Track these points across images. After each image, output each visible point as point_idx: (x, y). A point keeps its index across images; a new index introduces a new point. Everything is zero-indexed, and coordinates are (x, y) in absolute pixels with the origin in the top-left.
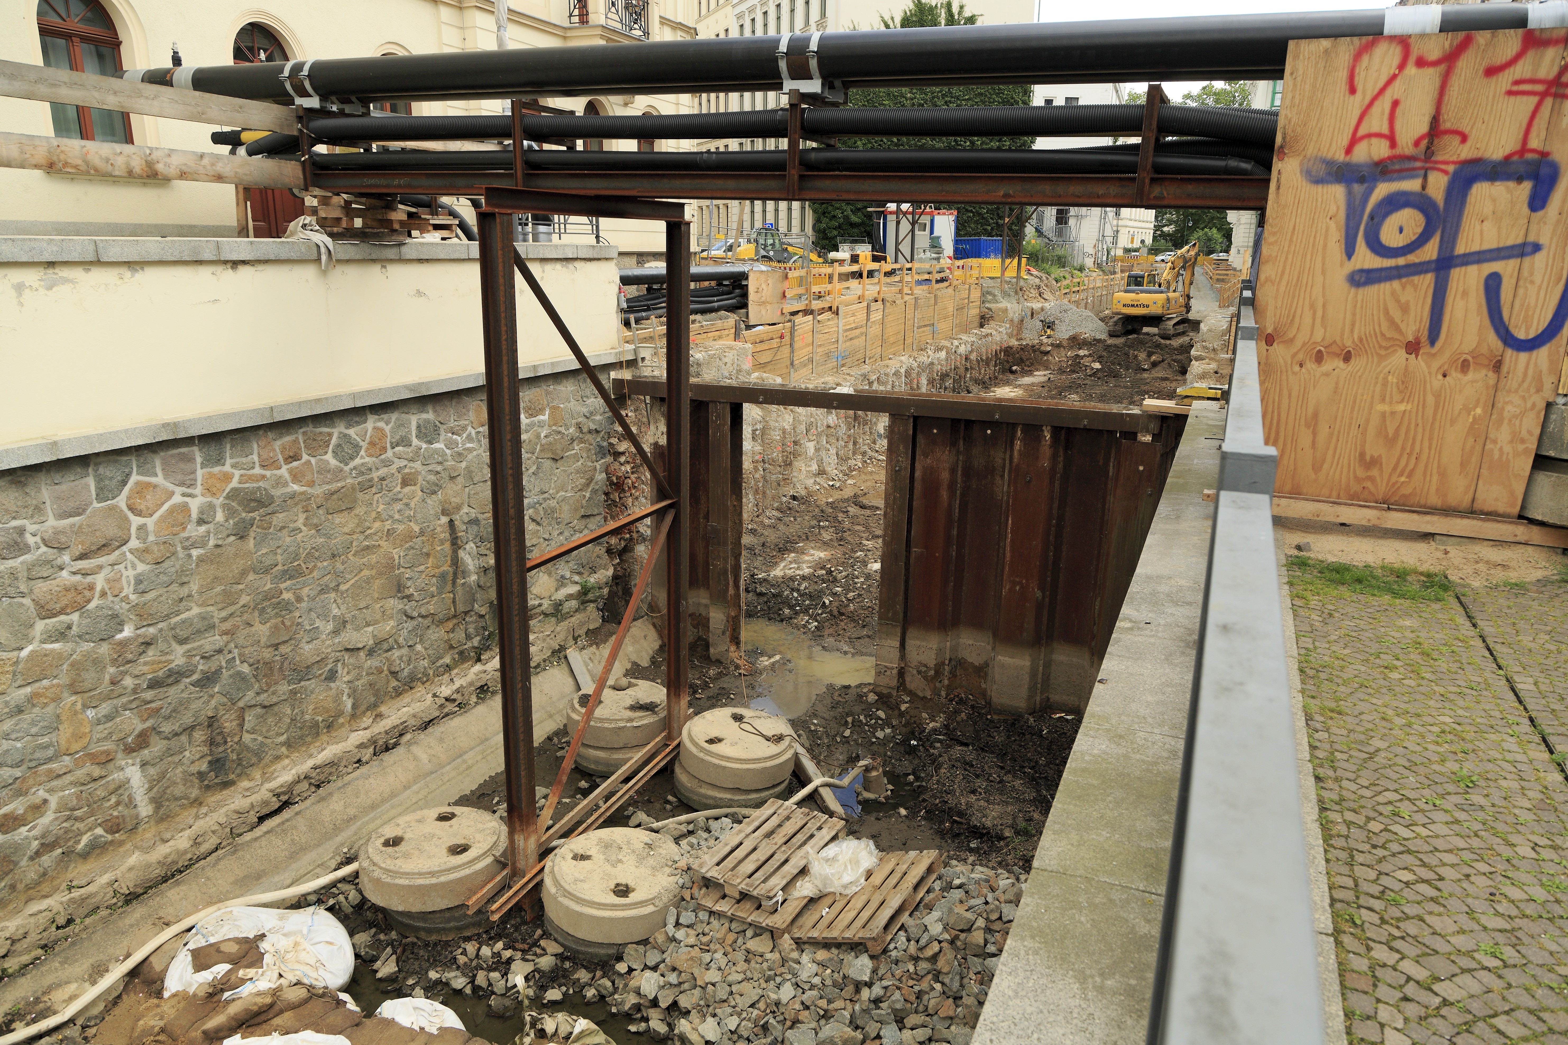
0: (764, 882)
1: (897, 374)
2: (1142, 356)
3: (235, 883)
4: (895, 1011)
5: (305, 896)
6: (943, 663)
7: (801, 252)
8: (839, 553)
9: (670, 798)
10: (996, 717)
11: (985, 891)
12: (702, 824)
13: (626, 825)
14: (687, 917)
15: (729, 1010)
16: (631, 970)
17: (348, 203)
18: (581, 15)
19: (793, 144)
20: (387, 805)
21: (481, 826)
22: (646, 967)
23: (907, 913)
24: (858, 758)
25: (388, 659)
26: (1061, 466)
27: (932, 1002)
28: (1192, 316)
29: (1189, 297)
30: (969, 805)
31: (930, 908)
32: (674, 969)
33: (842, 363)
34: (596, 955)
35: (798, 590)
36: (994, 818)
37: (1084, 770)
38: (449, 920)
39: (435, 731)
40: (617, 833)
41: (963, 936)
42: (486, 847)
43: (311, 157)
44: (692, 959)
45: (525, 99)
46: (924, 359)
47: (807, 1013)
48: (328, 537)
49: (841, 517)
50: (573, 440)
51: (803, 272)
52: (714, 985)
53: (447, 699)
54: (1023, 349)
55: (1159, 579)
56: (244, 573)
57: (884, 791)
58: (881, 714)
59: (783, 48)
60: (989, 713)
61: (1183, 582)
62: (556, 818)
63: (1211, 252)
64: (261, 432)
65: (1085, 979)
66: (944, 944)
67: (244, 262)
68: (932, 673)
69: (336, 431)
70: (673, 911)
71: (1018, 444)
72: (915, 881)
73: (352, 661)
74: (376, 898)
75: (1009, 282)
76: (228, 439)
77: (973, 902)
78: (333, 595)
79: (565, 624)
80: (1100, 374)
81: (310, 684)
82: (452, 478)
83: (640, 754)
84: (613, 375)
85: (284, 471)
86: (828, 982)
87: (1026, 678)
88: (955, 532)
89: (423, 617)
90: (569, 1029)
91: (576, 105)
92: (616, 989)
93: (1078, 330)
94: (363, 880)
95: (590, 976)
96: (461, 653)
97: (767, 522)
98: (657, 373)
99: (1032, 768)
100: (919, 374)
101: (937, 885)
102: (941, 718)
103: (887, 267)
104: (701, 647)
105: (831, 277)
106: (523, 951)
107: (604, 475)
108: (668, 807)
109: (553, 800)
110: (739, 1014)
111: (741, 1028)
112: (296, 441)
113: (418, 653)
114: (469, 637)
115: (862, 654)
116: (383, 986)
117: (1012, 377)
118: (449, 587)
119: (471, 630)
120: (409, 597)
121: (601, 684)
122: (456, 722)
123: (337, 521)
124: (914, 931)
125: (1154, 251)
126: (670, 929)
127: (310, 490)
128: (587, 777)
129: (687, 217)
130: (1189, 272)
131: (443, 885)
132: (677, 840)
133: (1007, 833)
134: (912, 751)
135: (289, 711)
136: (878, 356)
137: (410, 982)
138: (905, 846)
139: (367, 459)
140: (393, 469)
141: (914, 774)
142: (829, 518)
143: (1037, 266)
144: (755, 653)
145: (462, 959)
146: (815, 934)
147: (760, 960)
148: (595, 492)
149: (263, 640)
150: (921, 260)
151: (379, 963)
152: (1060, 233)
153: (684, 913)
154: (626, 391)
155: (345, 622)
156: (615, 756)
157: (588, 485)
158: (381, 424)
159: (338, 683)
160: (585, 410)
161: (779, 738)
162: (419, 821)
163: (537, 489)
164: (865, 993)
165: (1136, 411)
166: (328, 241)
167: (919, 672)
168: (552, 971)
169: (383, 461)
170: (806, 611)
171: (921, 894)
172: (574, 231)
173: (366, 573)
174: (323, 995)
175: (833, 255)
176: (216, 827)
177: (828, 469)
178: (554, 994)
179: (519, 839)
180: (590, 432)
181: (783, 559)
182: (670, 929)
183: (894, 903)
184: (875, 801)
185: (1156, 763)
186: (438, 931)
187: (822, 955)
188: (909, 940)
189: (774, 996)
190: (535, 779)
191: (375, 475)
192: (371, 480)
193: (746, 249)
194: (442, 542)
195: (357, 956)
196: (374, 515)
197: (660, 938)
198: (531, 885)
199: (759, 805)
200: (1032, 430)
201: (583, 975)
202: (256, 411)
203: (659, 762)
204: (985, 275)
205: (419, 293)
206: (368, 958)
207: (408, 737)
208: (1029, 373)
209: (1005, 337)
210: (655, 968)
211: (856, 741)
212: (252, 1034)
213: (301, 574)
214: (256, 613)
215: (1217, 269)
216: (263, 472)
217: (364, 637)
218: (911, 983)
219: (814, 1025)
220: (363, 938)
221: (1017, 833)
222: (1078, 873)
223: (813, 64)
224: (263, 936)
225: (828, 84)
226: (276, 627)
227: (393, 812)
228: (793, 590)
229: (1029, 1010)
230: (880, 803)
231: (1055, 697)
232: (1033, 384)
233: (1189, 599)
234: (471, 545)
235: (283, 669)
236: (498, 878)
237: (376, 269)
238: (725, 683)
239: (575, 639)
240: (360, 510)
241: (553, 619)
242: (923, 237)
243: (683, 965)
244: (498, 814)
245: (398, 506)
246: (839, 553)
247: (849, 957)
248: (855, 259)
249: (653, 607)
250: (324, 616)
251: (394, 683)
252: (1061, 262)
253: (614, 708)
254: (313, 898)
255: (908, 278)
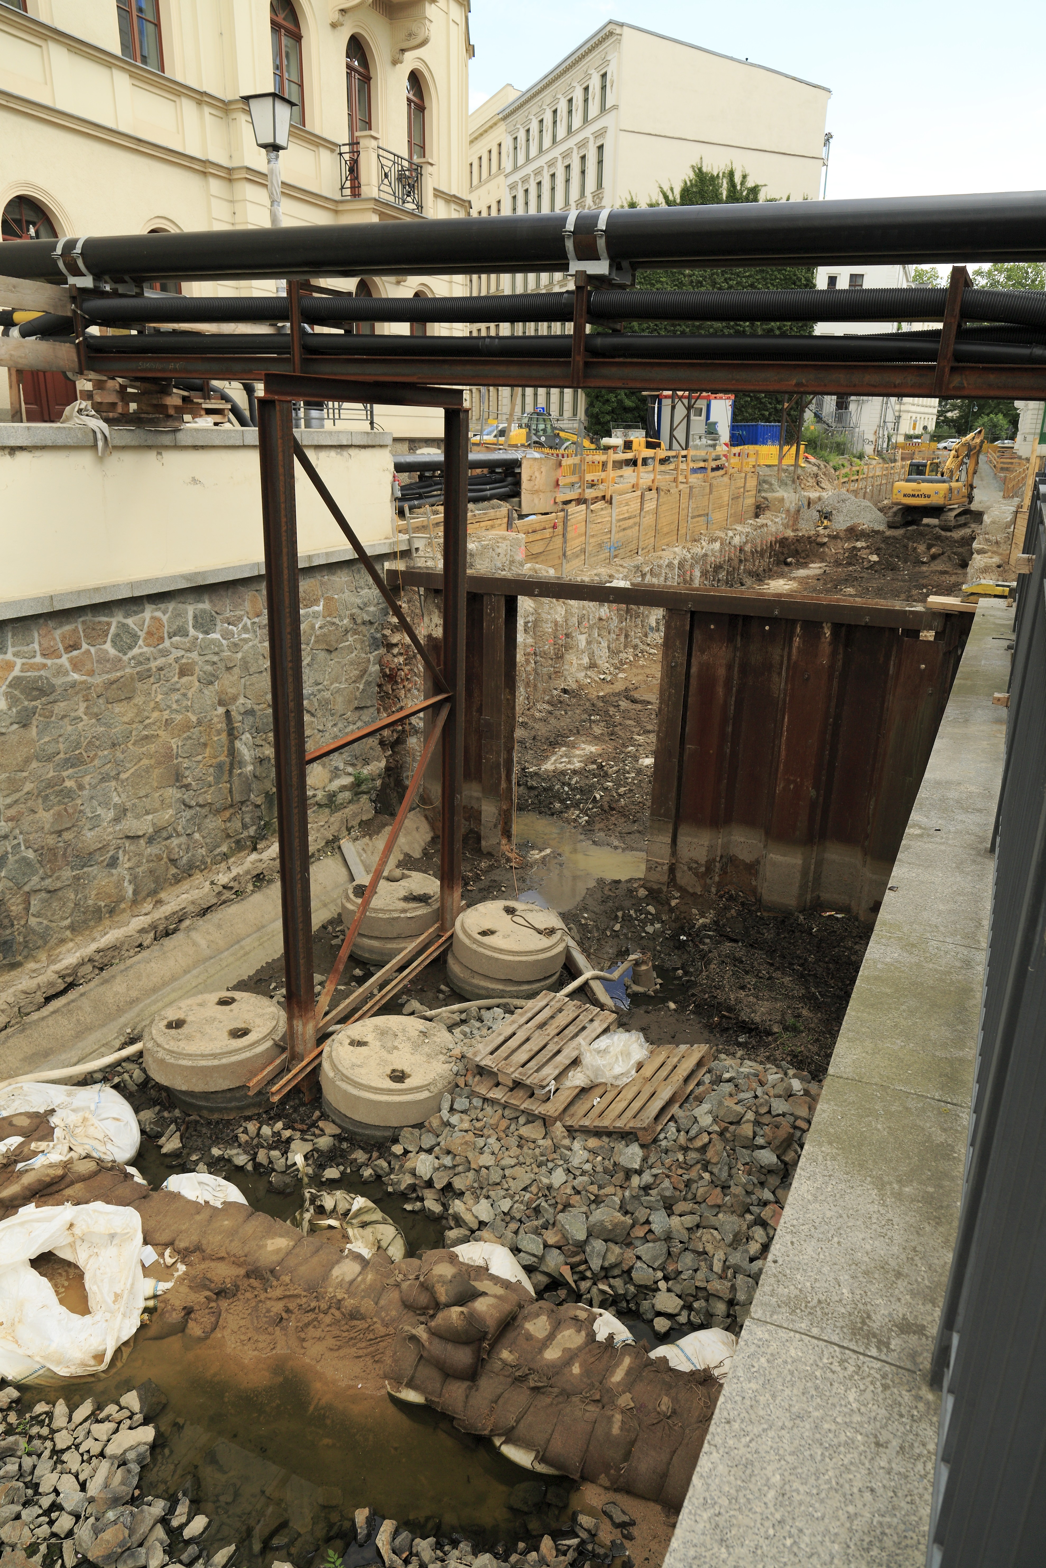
0: (537, 1071)
1: (670, 565)
2: (921, 548)
3: (24, 1060)
4: (664, 1198)
5: (91, 1073)
6: (714, 860)
7: (575, 438)
8: (610, 747)
9: (443, 987)
10: (765, 914)
11: (754, 1085)
12: (474, 1014)
13: (399, 1013)
14: (461, 1103)
15: (503, 1193)
16: (406, 1152)
17: (123, 388)
18: (352, 188)
19: (579, 329)
20: (168, 988)
21: (260, 1011)
22: (421, 1149)
23: (677, 1105)
24: (627, 952)
25: (167, 847)
26: (840, 663)
27: (701, 1191)
28: (974, 507)
29: (972, 487)
30: (738, 1001)
31: (700, 1100)
32: (448, 1152)
33: (614, 553)
34: (373, 1137)
35: (569, 785)
36: (763, 1014)
37: (876, 978)
38: (231, 1100)
39: (214, 917)
40: (392, 1021)
41: (732, 1128)
42: (265, 1030)
43: (85, 339)
44: (466, 1143)
45: (297, 278)
46: (698, 550)
47: (578, 1197)
48: (109, 726)
49: (612, 711)
50: (347, 631)
51: (576, 460)
52: (487, 1168)
53: (224, 887)
54: (799, 540)
55: (948, 784)
56: (27, 761)
57: (653, 984)
58: (651, 909)
59: (570, 226)
60: (759, 910)
61: (972, 788)
62: (333, 1005)
63: (996, 439)
64: (41, 621)
65: (883, 1185)
66: (714, 1136)
67: (21, 448)
68: (703, 869)
69: (115, 621)
70: (448, 1097)
71: (797, 640)
72: (685, 1074)
73: (132, 848)
74: (160, 1077)
75: (786, 471)
76: (9, 628)
77: (742, 1096)
78: (113, 784)
79: (338, 815)
80: (877, 567)
81: (93, 870)
82: (228, 669)
83: (414, 944)
84: (387, 565)
85: (64, 660)
86: (599, 1169)
87: (798, 876)
88: (730, 729)
89: (201, 806)
90: (347, 1206)
91: (347, 284)
92: (392, 1170)
93: (856, 521)
94: (148, 1060)
95: (367, 1156)
96: (238, 842)
97: (538, 715)
98: (430, 564)
99: (801, 965)
100: (692, 566)
101: (707, 1079)
102: (711, 914)
103: (662, 453)
104: (474, 839)
105: (604, 465)
106: (303, 1132)
107: (377, 667)
108: (441, 996)
109: (330, 987)
110: (512, 1197)
111: (514, 1210)
112: (75, 630)
113: (196, 841)
114: (245, 826)
115: (633, 849)
116: (167, 1161)
117: (786, 569)
118: (226, 777)
119: (247, 820)
120: (187, 787)
121: (377, 877)
122: (233, 910)
123: (117, 710)
124: (684, 1122)
125: (937, 437)
126: (445, 1114)
127: (89, 679)
128: (363, 966)
129: (466, 405)
130: (973, 461)
131: (225, 1067)
132: (450, 1028)
133: (775, 1029)
134: (681, 946)
135: (72, 896)
136: (651, 547)
137: (194, 1158)
138: (674, 1039)
139: (145, 649)
140: (171, 659)
141: (682, 968)
142: (601, 712)
143: (815, 454)
144: (526, 846)
145: (243, 1138)
146: (586, 1122)
147: (532, 1146)
148: (368, 683)
149: (47, 827)
150: (697, 447)
151: (163, 1139)
152: (839, 419)
153: (458, 1099)
154: (400, 582)
155: (125, 810)
156: (389, 946)
157: (362, 676)
158: (158, 614)
159: (119, 869)
160: (359, 601)
161: (551, 932)
162: (200, 1005)
163: (312, 681)
164: (635, 1181)
165: (919, 608)
166: (104, 426)
167: (690, 869)
168: (331, 1151)
169: (160, 651)
170: (576, 805)
171: (691, 1087)
172: (348, 418)
173: (145, 762)
174: (112, 1169)
175: (606, 441)
176: (5, 1007)
177: (599, 662)
178: (332, 1173)
179: (298, 1025)
180: (364, 623)
181: (554, 753)
182: (445, 1114)
183: (665, 1094)
184: (644, 995)
185: (950, 973)
186: (220, 1110)
187: (593, 1142)
188: (678, 1131)
189: (546, 1181)
190: (313, 966)
191: (154, 665)
192: (149, 670)
193: (517, 434)
194: (219, 733)
195: (143, 1132)
196: (152, 704)
197: (435, 1123)
198: (309, 1069)
199: (532, 995)
200: (812, 627)
201: (360, 1156)
202: (37, 600)
203: (432, 952)
204: (762, 462)
205: (195, 481)
206: (153, 1134)
207: (187, 923)
208: (805, 565)
209: (781, 528)
210: (429, 1151)
211: (625, 935)
212: (45, 1204)
213: (83, 763)
214: (40, 801)
215: (1001, 457)
216: (45, 661)
217: (143, 825)
218: (680, 1171)
219: (584, 1209)
220: (148, 1115)
221: (786, 1029)
222: (874, 1081)
223: (601, 243)
224: (53, 1111)
225: (615, 265)
226: (59, 814)
227: (173, 996)
228: (564, 784)
229: (829, 1214)
230: (649, 996)
231: (825, 896)
232: (808, 577)
233: (979, 807)
234: (247, 736)
235: (65, 855)
236: (278, 1061)
237: (151, 457)
238: (496, 875)
239: (349, 830)
240: (139, 700)
241: (327, 810)
242: (698, 424)
243: (458, 1149)
244: (275, 999)
245: (176, 696)
246: (610, 747)
247: (620, 1146)
248: (628, 445)
249: (424, 799)
250: (106, 804)
251: (173, 870)
252: (840, 449)
253: (388, 898)
254: (99, 1076)
255: (683, 466)
